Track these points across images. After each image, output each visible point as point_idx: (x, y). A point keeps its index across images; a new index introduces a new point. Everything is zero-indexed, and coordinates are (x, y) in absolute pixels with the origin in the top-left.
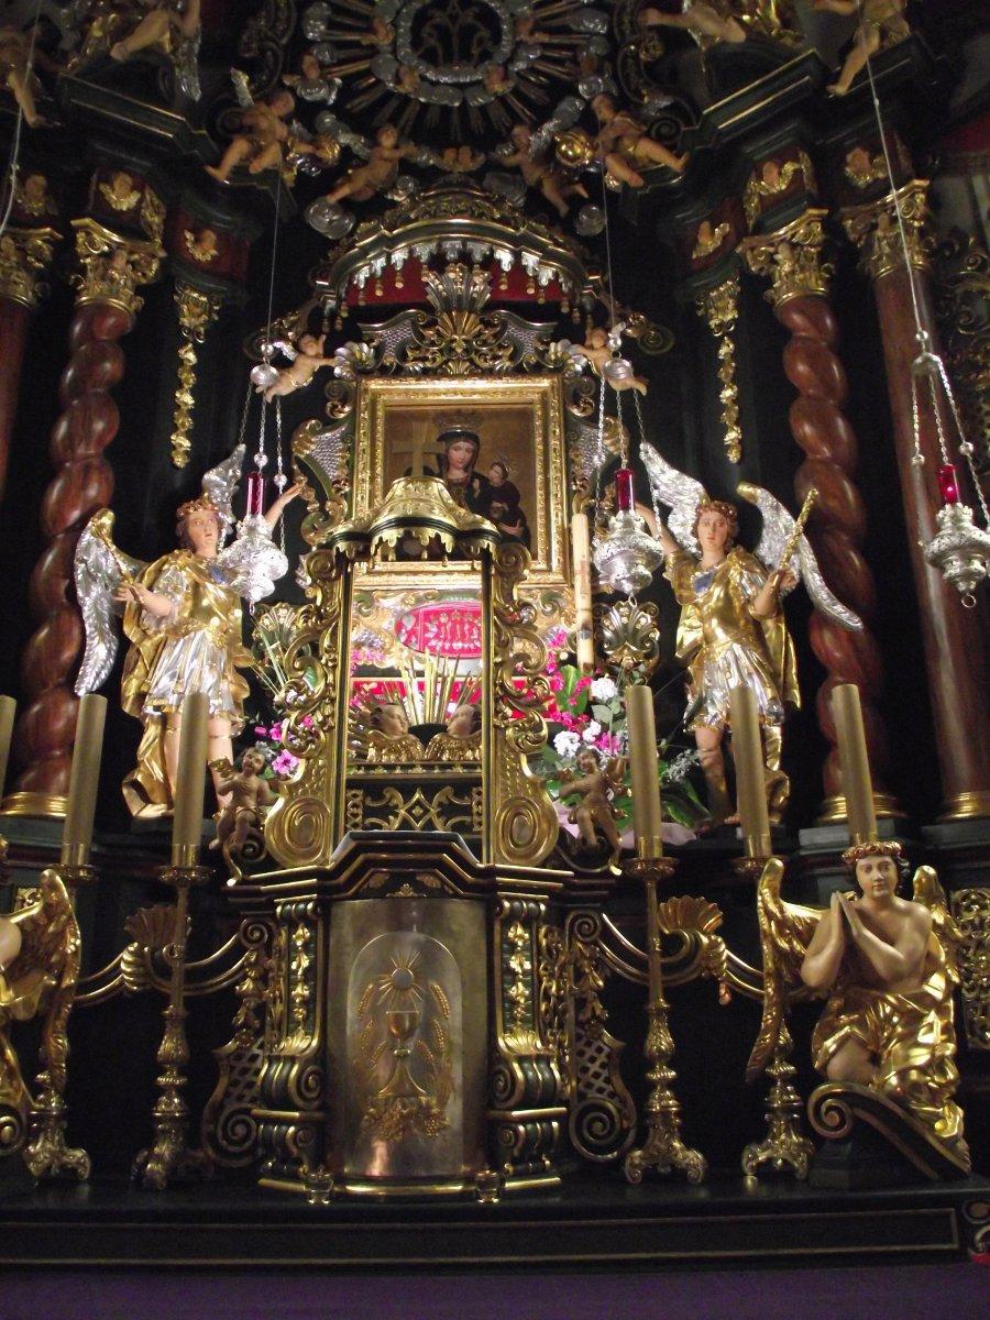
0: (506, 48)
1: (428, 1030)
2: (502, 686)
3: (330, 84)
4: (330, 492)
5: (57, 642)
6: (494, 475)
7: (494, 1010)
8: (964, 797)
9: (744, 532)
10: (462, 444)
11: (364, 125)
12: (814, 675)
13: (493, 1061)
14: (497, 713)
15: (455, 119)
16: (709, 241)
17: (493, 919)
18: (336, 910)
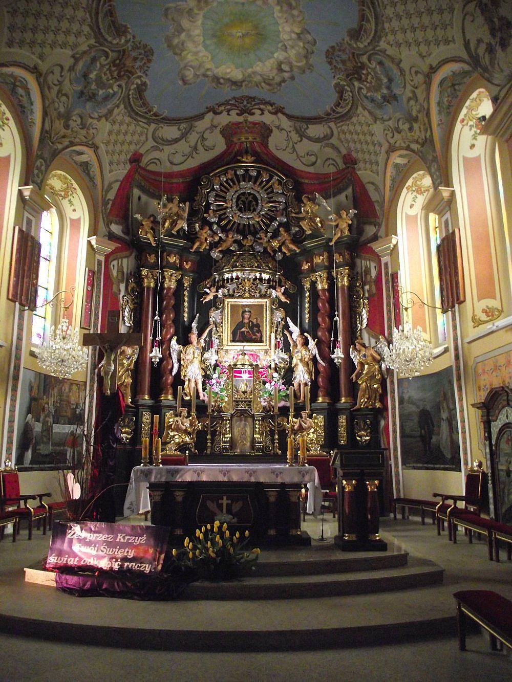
0: (259, 208)
1: (245, 435)
3: (216, 217)
4: (218, 325)
5: (168, 363)
6: (255, 321)
7: (254, 432)
8: (343, 398)
9: (306, 343)
10: (247, 313)
11: (224, 229)
12: (317, 372)
13: (254, 438)
15: (247, 227)
16: (306, 267)
17: (254, 420)
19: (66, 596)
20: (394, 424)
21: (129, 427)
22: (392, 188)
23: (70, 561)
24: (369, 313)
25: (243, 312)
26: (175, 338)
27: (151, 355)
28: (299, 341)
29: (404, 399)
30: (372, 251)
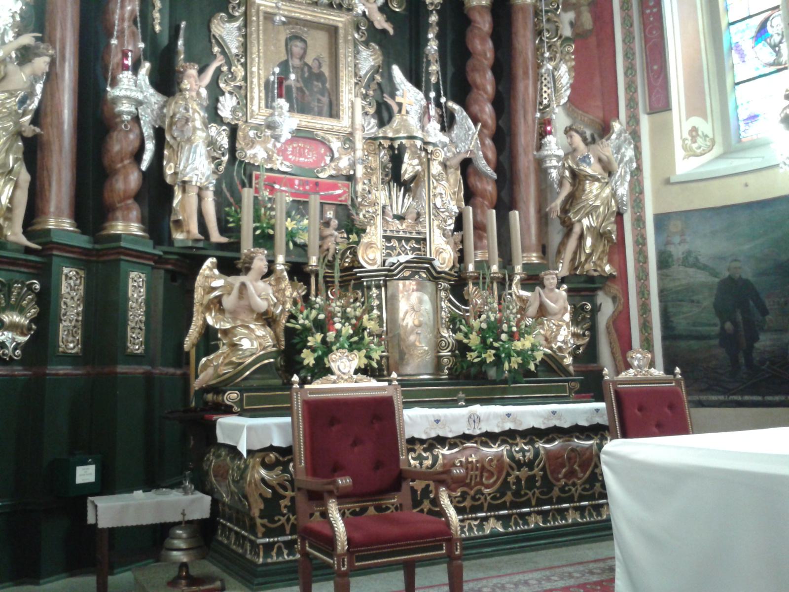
19: (752, 115)
20: (645, 308)
21: (21, 311)
22: (232, 196)
24: (575, 71)
25: (288, 41)
29: (670, 255)
30: (477, 27)
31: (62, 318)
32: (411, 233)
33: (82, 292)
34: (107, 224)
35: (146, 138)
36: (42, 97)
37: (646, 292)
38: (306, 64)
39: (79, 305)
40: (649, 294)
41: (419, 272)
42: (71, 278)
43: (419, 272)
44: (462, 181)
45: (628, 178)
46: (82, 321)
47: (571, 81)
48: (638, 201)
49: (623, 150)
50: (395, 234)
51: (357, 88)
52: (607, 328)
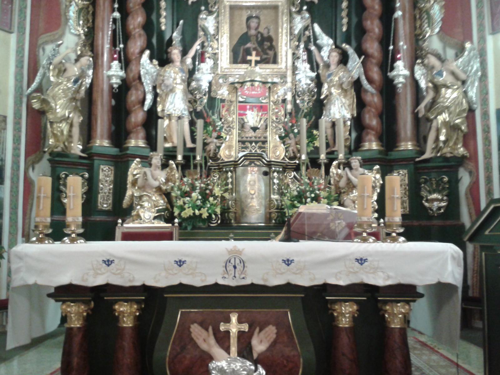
2: (273, 119)
9: (344, 59)
14: (272, 125)
18: (237, 169)
23: (355, 162)
24: (445, 9)
25: (249, 18)
26: (147, 52)
27: (110, 73)
28: (335, 57)
31: (100, 191)
32: (259, 138)
33: (112, 178)
34: (127, 141)
35: (146, 93)
36: (93, 77)
37: (490, 167)
38: (259, 32)
39: (110, 185)
40: (492, 169)
41: (254, 162)
42: (105, 171)
43: (254, 162)
44: (355, 97)
45: (476, 84)
46: (112, 193)
47: (442, 16)
48: (485, 100)
49: (472, 63)
50: (249, 139)
51: (292, 42)
52: (466, 194)
